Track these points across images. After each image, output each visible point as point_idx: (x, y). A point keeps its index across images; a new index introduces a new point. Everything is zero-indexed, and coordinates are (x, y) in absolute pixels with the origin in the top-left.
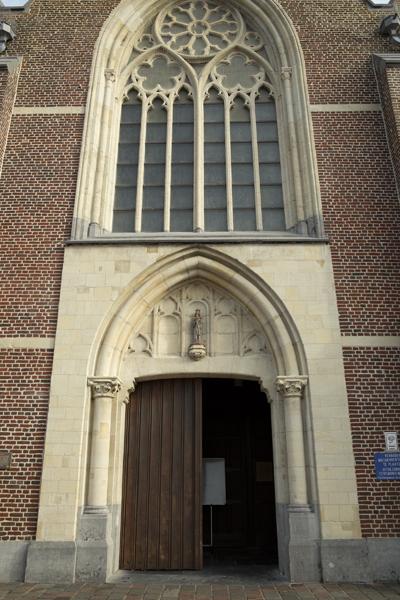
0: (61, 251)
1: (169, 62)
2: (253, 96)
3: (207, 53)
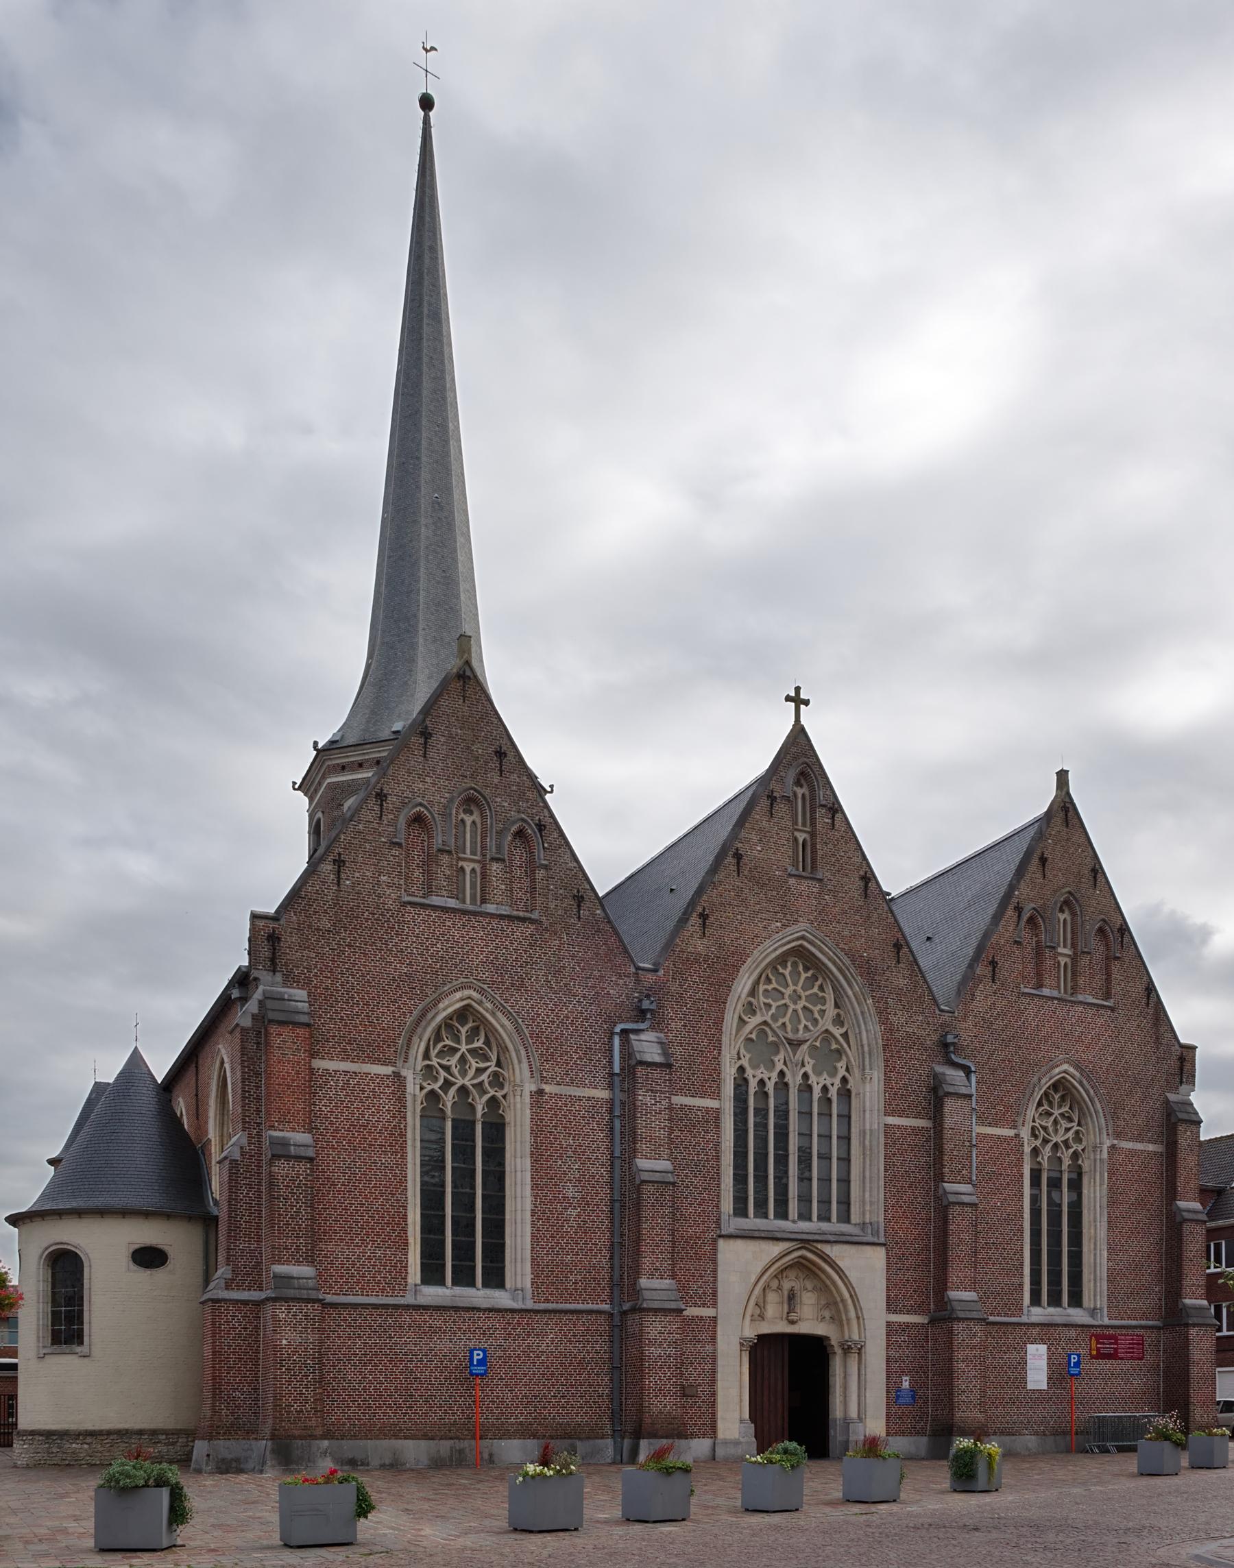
0: (715, 1241)
1: (771, 1039)
2: (836, 1087)
3: (801, 1035)
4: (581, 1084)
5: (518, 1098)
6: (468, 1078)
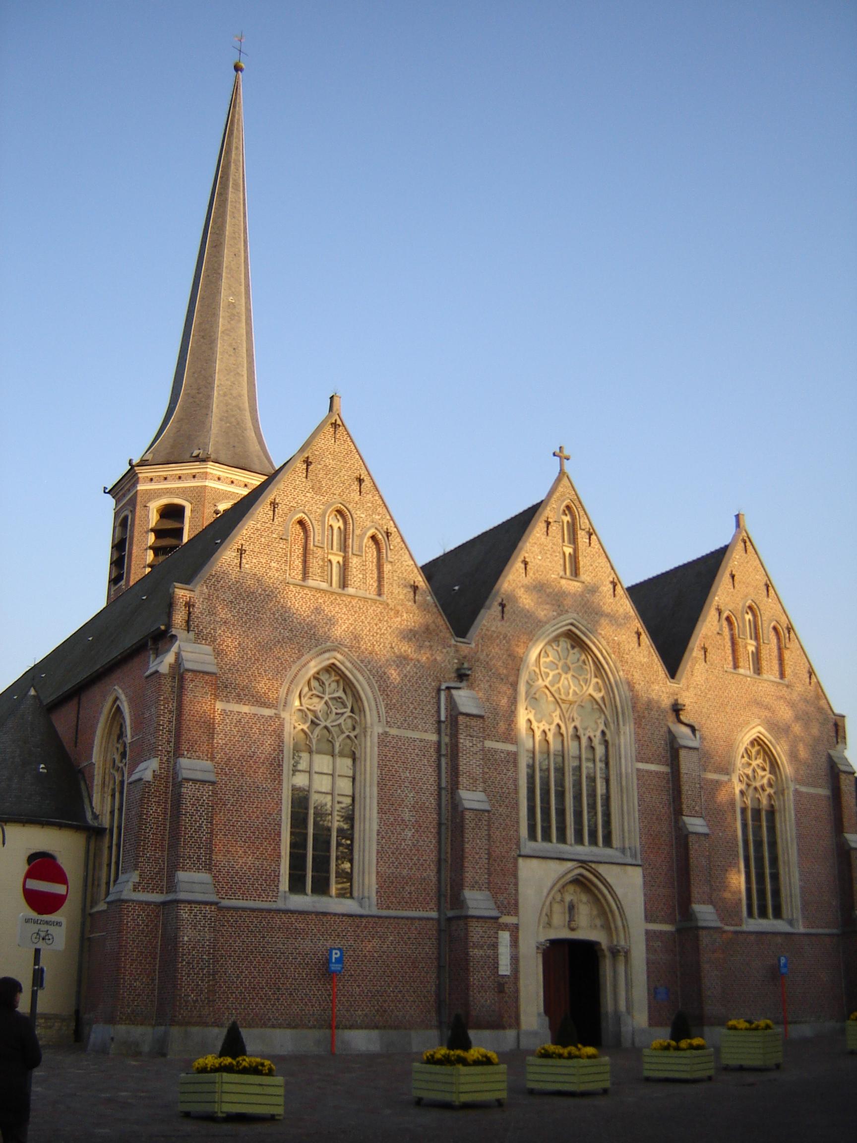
4: (415, 728)
5: (368, 738)
6: (329, 721)
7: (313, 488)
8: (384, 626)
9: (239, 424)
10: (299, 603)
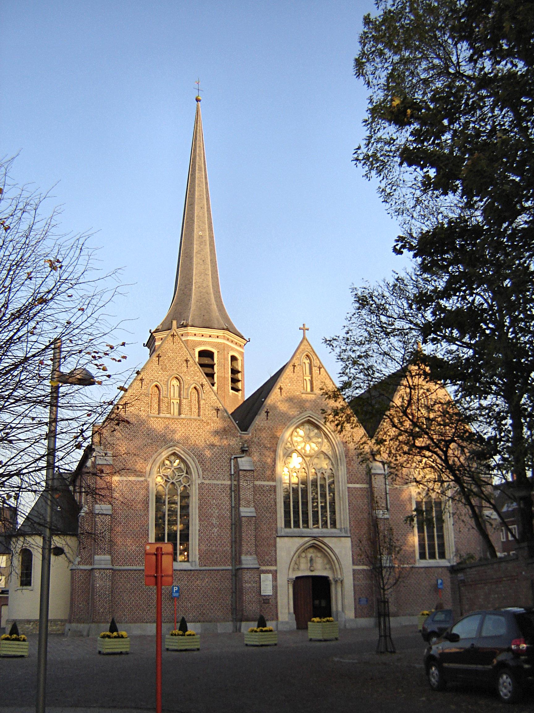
0: (275, 539)
5: (194, 486)
7: (162, 369)
8: (201, 431)
9: (208, 303)
10: (157, 425)
